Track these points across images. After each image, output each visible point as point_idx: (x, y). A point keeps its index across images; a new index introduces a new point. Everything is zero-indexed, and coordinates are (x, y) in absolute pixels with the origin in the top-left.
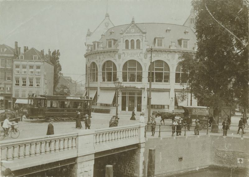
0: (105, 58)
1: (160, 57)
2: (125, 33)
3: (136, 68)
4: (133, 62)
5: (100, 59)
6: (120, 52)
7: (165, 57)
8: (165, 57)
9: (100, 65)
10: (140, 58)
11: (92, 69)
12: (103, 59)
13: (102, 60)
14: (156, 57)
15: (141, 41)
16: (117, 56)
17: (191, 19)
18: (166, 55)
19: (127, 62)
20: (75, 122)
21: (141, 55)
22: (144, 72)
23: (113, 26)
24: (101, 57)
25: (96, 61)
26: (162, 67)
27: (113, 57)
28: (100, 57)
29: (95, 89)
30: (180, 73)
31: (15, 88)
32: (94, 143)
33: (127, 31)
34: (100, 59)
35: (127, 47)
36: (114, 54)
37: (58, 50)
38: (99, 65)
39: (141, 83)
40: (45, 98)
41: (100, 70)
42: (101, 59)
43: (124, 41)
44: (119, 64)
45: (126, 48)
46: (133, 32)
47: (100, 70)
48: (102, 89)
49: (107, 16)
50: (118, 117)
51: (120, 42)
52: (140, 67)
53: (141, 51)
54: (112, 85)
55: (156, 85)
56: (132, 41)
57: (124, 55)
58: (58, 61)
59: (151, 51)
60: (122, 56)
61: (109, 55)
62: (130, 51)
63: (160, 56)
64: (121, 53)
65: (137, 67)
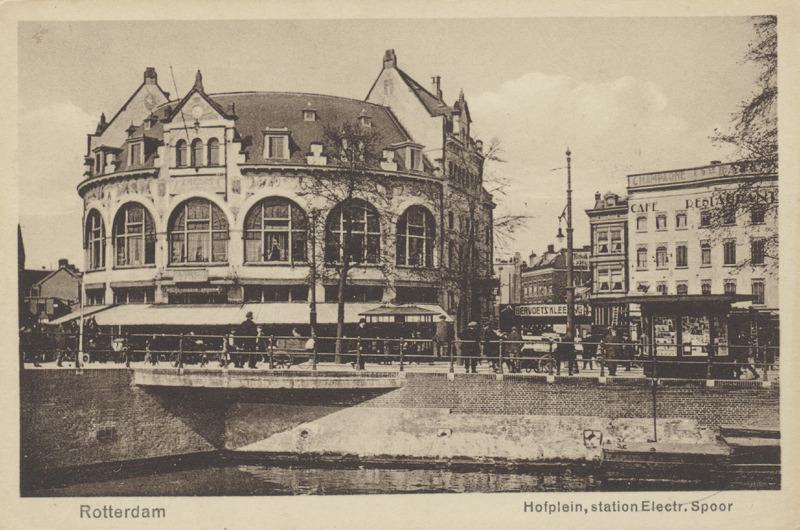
6: (164, 174)
17: (386, 81)
43: (174, 143)
49: (151, 74)
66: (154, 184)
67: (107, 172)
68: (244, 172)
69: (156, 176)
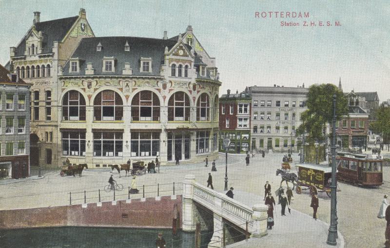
3: (78, 102)
6: (167, 79)
11: (201, 102)
12: (64, 88)
14: (71, 86)
16: (160, 84)
19: (101, 92)
20: (330, 200)
22: (88, 106)
25: (82, 89)
26: (181, 100)
30: (183, 108)
33: (174, 52)
35: (173, 74)
36: (81, 82)
38: (127, 97)
39: (84, 121)
43: (171, 65)
45: (172, 75)
50: (280, 176)
61: (148, 82)
65: (80, 101)
67: (86, 74)
69: (161, 79)
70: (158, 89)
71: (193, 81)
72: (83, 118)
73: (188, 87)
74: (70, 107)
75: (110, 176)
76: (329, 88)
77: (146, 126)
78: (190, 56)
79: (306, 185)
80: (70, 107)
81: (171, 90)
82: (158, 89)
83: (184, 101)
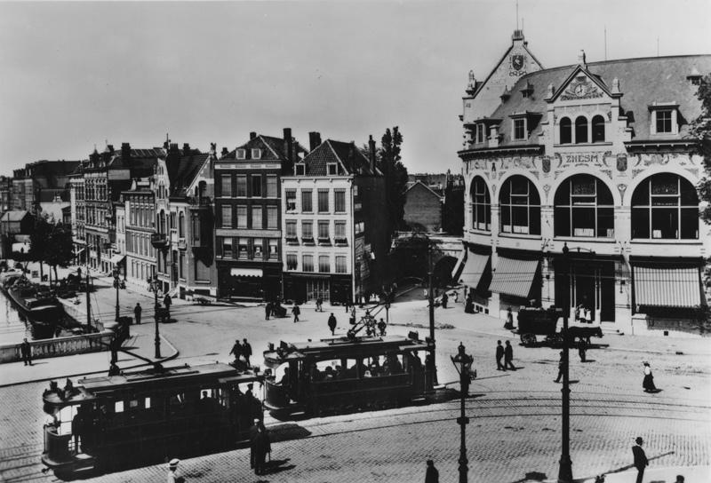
0: (507, 168)
1: (666, 162)
2: (559, 98)
4: (583, 182)
5: (494, 168)
7: (683, 164)
8: (683, 164)
9: (495, 184)
10: (604, 168)
12: (639, 167)
13: (502, 174)
15: (606, 118)
18: (687, 156)
21: (607, 159)
22: (619, 208)
23: (538, 68)
24: (498, 163)
27: (528, 167)
28: (494, 164)
29: (483, 250)
31: (287, 249)
32: (462, 395)
33: (563, 93)
34: (494, 168)
35: (565, 138)
37: (396, 129)
38: (547, 188)
40: (313, 355)
41: (495, 199)
42: (498, 170)
43: (558, 121)
44: (547, 187)
46: (583, 94)
47: (495, 199)
48: (504, 253)
51: (548, 124)
52: (535, 197)
53: (606, 149)
54: (521, 239)
55: (656, 247)
56: (582, 120)
57: (558, 160)
58: (399, 158)
59: (636, 148)
60: (554, 163)
62: (573, 149)
63: (666, 159)
64: (552, 155)
66: (539, 162)
68: (629, 150)
70: (534, 173)
71: (620, 149)
72: (536, 229)
73: (602, 163)
74: (682, 209)
75: (497, 345)
76: (383, 138)
77: (518, 244)
78: (605, 94)
79: (76, 446)
80: (653, 209)
81: (639, 171)
82: (534, 173)
83: (679, 194)
